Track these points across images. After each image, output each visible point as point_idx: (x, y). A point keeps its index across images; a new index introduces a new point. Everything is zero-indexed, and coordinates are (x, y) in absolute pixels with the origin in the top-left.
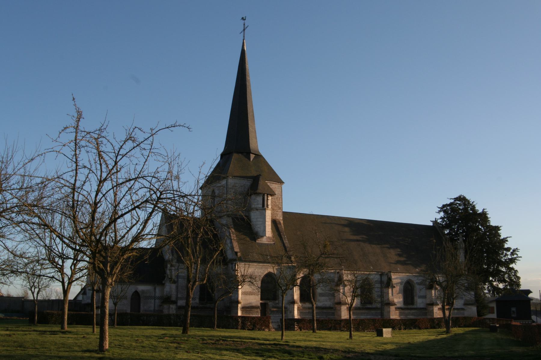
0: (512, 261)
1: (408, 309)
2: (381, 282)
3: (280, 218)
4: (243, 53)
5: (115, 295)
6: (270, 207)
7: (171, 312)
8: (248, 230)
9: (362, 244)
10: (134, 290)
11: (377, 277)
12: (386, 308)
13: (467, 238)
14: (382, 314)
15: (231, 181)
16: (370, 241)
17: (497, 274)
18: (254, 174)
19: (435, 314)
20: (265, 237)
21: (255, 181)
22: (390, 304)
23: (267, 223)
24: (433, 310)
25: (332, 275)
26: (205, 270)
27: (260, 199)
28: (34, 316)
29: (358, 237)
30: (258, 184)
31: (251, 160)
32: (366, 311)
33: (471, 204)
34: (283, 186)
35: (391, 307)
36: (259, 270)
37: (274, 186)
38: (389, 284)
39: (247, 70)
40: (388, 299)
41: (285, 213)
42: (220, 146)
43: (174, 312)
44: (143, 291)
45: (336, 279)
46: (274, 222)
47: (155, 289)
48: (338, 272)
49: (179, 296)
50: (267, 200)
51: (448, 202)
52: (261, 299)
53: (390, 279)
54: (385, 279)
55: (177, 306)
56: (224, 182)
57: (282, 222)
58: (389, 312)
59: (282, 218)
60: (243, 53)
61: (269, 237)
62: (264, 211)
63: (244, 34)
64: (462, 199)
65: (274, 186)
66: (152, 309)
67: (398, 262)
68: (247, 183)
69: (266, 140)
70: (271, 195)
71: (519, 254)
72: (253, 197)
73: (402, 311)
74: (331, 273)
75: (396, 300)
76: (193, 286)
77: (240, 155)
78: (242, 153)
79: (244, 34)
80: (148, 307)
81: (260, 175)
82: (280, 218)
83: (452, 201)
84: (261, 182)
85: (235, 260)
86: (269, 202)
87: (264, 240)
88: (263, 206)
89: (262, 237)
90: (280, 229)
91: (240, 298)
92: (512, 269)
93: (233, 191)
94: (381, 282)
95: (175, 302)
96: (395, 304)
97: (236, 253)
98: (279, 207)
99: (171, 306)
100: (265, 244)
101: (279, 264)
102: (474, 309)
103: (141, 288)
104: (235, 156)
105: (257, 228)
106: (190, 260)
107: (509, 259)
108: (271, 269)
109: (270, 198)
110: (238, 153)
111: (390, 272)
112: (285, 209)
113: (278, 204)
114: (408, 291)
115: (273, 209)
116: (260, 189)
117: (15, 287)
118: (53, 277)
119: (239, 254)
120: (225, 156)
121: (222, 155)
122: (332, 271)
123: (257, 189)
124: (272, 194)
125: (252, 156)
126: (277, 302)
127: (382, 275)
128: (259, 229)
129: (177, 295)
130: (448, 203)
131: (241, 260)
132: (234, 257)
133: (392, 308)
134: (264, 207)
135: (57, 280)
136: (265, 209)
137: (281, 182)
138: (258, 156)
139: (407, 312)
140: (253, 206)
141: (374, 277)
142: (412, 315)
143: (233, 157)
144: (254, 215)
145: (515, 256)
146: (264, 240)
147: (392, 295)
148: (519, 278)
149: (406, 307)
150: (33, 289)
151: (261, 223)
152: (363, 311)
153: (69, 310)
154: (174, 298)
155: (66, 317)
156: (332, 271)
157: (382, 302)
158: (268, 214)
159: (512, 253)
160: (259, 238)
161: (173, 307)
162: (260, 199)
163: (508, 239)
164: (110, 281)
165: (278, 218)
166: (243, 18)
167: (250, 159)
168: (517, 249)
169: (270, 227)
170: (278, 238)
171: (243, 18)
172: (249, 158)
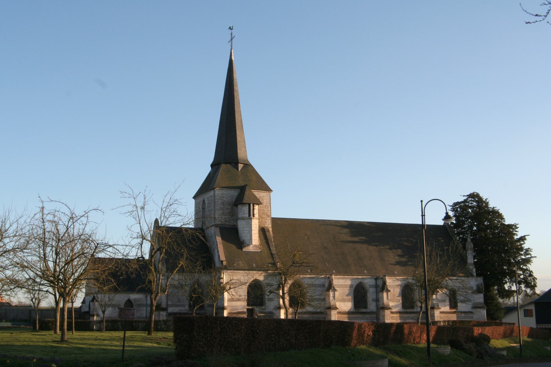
0: (528, 261)
1: (407, 313)
2: (376, 286)
3: (268, 225)
4: (231, 62)
5: (103, 303)
6: (257, 216)
7: (161, 318)
8: (233, 235)
9: (358, 246)
10: (126, 299)
11: (372, 282)
12: (381, 311)
13: (479, 239)
14: (378, 318)
15: (218, 192)
16: (368, 242)
17: (512, 275)
18: (242, 183)
19: (436, 317)
20: (251, 246)
21: (242, 189)
22: (385, 308)
23: (253, 232)
24: (434, 314)
25: (322, 280)
26: (166, 284)
27: (246, 208)
28: (36, 324)
29: (356, 239)
30: (244, 193)
31: (239, 170)
32: (360, 316)
33: (484, 202)
34: (272, 194)
35: (386, 311)
36: (245, 277)
37: (258, 194)
38: (383, 288)
39: (235, 80)
40: (383, 303)
41: (275, 221)
42: (211, 157)
43: (165, 318)
44: (135, 300)
45: (327, 285)
46: (263, 231)
47: (146, 297)
48: (328, 278)
49: (169, 303)
50: (253, 209)
51: (462, 199)
52: (248, 305)
53: (384, 283)
54: (380, 283)
55: (167, 312)
56: (212, 193)
57: (271, 229)
58: (384, 316)
59: (270, 226)
60: (231, 62)
61: (255, 246)
62: (250, 220)
63: (232, 44)
64: (474, 196)
65: (258, 194)
66: (144, 316)
67: (398, 263)
68: (235, 193)
69: (255, 149)
70: (258, 204)
71: (533, 254)
72: (239, 206)
73: (402, 315)
74: (322, 278)
75: (391, 304)
76: (156, 297)
77: (228, 165)
78: (230, 163)
79: (232, 44)
80: (141, 313)
81: (246, 185)
82: (268, 225)
83: (465, 198)
84: (247, 193)
85: (222, 269)
86: (256, 212)
87: (251, 248)
88: (249, 215)
89: (249, 245)
90: (268, 236)
91: (226, 304)
92: (527, 270)
93: (221, 201)
94: (376, 286)
95: (165, 309)
96: (390, 308)
97: (222, 262)
98: (267, 215)
99: (161, 313)
100: (252, 252)
101: (265, 271)
102: (484, 312)
103: (134, 296)
104: (223, 167)
105: (243, 235)
106: (153, 276)
107: (522, 259)
108: (260, 276)
109: (256, 207)
110: (226, 163)
111: (385, 276)
112: (274, 215)
113: (266, 212)
114: (407, 293)
115: (260, 217)
116: (246, 200)
117: (20, 297)
118: (47, 291)
119: (225, 263)
120: (215, 165)
121: (212, 166)
122: (323, 276)
123: (242, 200)
124: (259, 203)
125: (240, 166)
126: (264, 307)
127: (376, 279)
128: (245, 238)
129: (167, 303)
130: (463, 200)
131: (226, 268)
132: (221, 266)
133: (387, 312)
134: (250, 215)
135: (50, 293)
136: (251, 219)
137: (268, 190)
138: (247, 165)
139: (406, 315)
140: (240, 216)
141: (368, 281)
142: (412, 319)
143: (221, 168)
144: (241, 225)
145: (529, 256)
146: (251, 248)
147: (388, 299)
148: (535, 279)
149: (403, 311)
150: (34, 300)
151: (247, 232)
152: (357, 316)
153: (68, 318)
154: (164, 306)
155: (66, 324)
156: (323, 276)
157: (377, 306)
158: (255, 224)
159: (525, 252)
160: (245, 247)
161: (163, 313)
162: (246, 208)
163: (526, 237)
164: (67, 299)
165: (266, 226)
166: (230, 28)
167: (238, 169)
168: (529, 248)
169: (257, 235)
170: (265, 244)
171: (230, 28)
172: (237, 168)
